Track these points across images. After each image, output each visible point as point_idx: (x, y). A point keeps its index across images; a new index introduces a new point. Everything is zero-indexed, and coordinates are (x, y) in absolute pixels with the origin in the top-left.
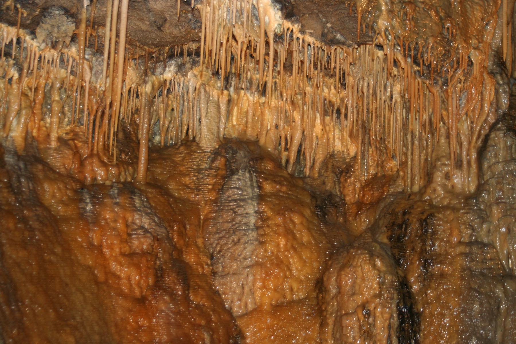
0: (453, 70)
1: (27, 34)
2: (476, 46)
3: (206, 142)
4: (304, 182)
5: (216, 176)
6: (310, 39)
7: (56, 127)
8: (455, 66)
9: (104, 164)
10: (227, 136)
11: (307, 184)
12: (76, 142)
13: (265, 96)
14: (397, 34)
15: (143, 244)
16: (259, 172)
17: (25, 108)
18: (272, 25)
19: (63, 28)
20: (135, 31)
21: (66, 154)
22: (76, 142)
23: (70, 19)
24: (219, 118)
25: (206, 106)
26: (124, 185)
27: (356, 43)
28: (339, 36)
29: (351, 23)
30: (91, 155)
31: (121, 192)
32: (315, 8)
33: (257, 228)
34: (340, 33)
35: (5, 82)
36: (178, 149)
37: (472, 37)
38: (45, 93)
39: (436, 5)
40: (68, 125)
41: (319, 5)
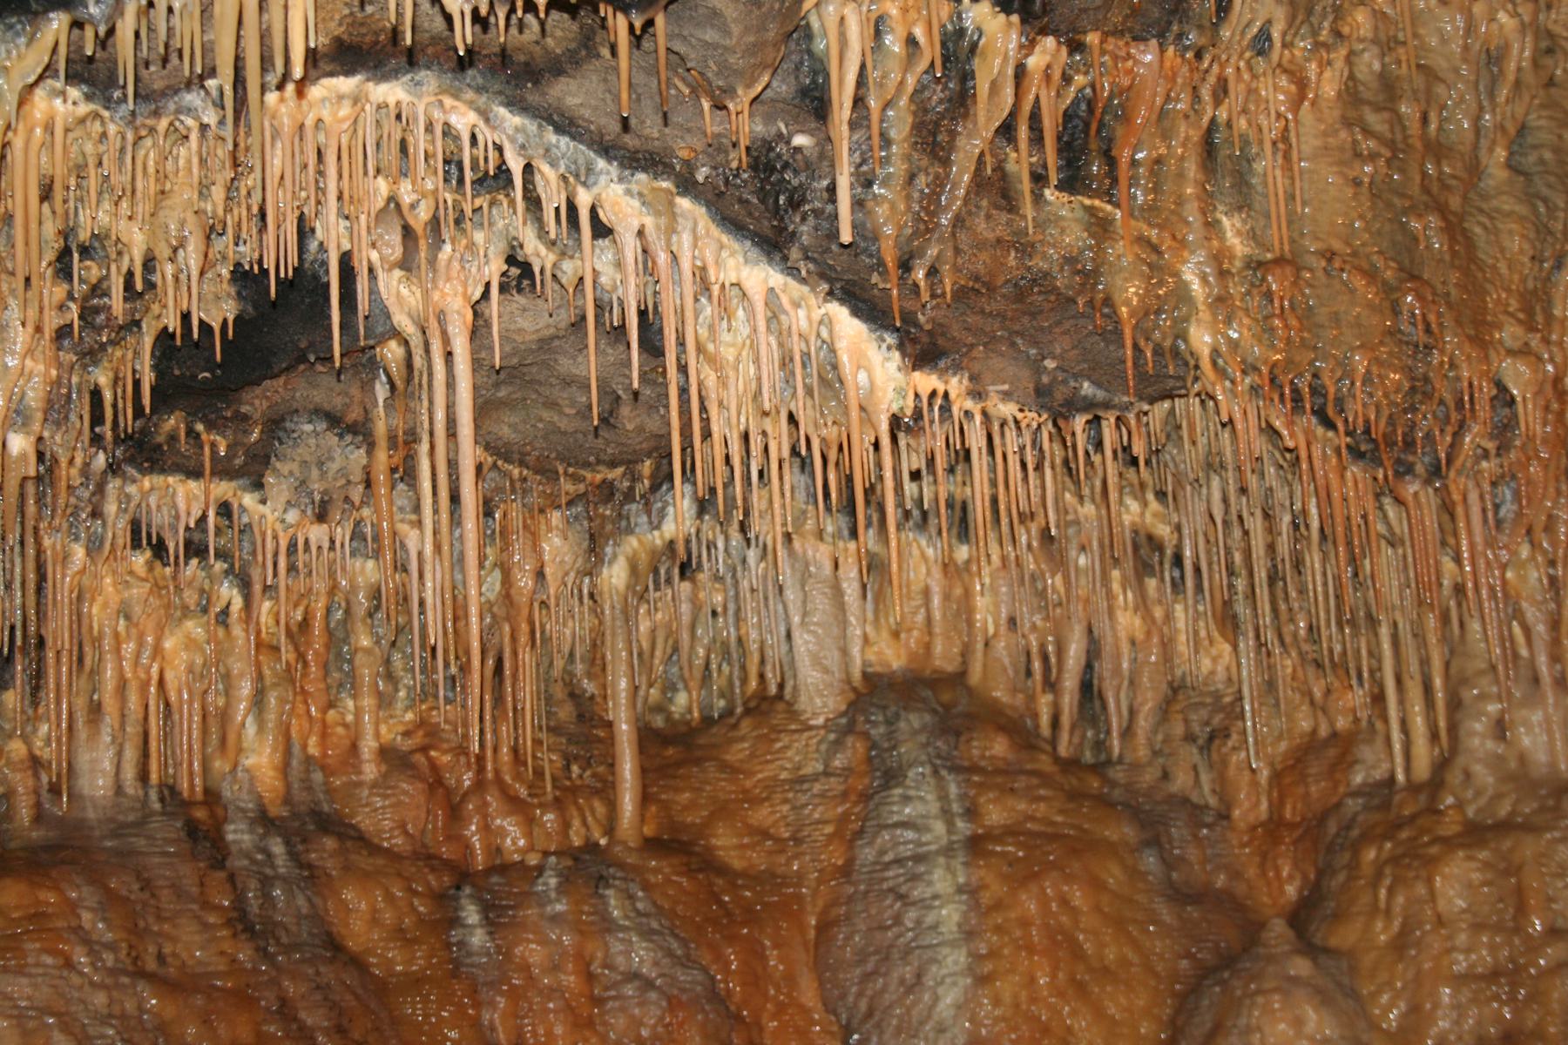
0: (1449, 429)
1: (244, 490)
2: (1516, 345)
3: (811, 699)
5: (845, 795)
7: (375, 724)
8: (1454, 416)
9: (515, 804)
10: (879, 669)
12: (433, 753)
13: (968, 542)
14: (1250, 360)
15: (640, 1024)
16: (965, 770)
17: (275, 685)
20: (545, 437)
21: (405, 793)
22: (433, 753)
23: (348, 438)
24: (844, 624)
25: (801, 595)
26: (576, 859)
27: (1141, 399)
28: (1087, 388)
29: (1112, 348)
30: (480, 785)
31: (566, 880)
32: (996, 326)
33: (969, 934)
34: (1089, 378)
35: (208, 623)
36: (735, 726)
37: (1502, 317)
38: (329, 632)
39: (1368, 249)
40: (407, 709)
41: (1004, 317)
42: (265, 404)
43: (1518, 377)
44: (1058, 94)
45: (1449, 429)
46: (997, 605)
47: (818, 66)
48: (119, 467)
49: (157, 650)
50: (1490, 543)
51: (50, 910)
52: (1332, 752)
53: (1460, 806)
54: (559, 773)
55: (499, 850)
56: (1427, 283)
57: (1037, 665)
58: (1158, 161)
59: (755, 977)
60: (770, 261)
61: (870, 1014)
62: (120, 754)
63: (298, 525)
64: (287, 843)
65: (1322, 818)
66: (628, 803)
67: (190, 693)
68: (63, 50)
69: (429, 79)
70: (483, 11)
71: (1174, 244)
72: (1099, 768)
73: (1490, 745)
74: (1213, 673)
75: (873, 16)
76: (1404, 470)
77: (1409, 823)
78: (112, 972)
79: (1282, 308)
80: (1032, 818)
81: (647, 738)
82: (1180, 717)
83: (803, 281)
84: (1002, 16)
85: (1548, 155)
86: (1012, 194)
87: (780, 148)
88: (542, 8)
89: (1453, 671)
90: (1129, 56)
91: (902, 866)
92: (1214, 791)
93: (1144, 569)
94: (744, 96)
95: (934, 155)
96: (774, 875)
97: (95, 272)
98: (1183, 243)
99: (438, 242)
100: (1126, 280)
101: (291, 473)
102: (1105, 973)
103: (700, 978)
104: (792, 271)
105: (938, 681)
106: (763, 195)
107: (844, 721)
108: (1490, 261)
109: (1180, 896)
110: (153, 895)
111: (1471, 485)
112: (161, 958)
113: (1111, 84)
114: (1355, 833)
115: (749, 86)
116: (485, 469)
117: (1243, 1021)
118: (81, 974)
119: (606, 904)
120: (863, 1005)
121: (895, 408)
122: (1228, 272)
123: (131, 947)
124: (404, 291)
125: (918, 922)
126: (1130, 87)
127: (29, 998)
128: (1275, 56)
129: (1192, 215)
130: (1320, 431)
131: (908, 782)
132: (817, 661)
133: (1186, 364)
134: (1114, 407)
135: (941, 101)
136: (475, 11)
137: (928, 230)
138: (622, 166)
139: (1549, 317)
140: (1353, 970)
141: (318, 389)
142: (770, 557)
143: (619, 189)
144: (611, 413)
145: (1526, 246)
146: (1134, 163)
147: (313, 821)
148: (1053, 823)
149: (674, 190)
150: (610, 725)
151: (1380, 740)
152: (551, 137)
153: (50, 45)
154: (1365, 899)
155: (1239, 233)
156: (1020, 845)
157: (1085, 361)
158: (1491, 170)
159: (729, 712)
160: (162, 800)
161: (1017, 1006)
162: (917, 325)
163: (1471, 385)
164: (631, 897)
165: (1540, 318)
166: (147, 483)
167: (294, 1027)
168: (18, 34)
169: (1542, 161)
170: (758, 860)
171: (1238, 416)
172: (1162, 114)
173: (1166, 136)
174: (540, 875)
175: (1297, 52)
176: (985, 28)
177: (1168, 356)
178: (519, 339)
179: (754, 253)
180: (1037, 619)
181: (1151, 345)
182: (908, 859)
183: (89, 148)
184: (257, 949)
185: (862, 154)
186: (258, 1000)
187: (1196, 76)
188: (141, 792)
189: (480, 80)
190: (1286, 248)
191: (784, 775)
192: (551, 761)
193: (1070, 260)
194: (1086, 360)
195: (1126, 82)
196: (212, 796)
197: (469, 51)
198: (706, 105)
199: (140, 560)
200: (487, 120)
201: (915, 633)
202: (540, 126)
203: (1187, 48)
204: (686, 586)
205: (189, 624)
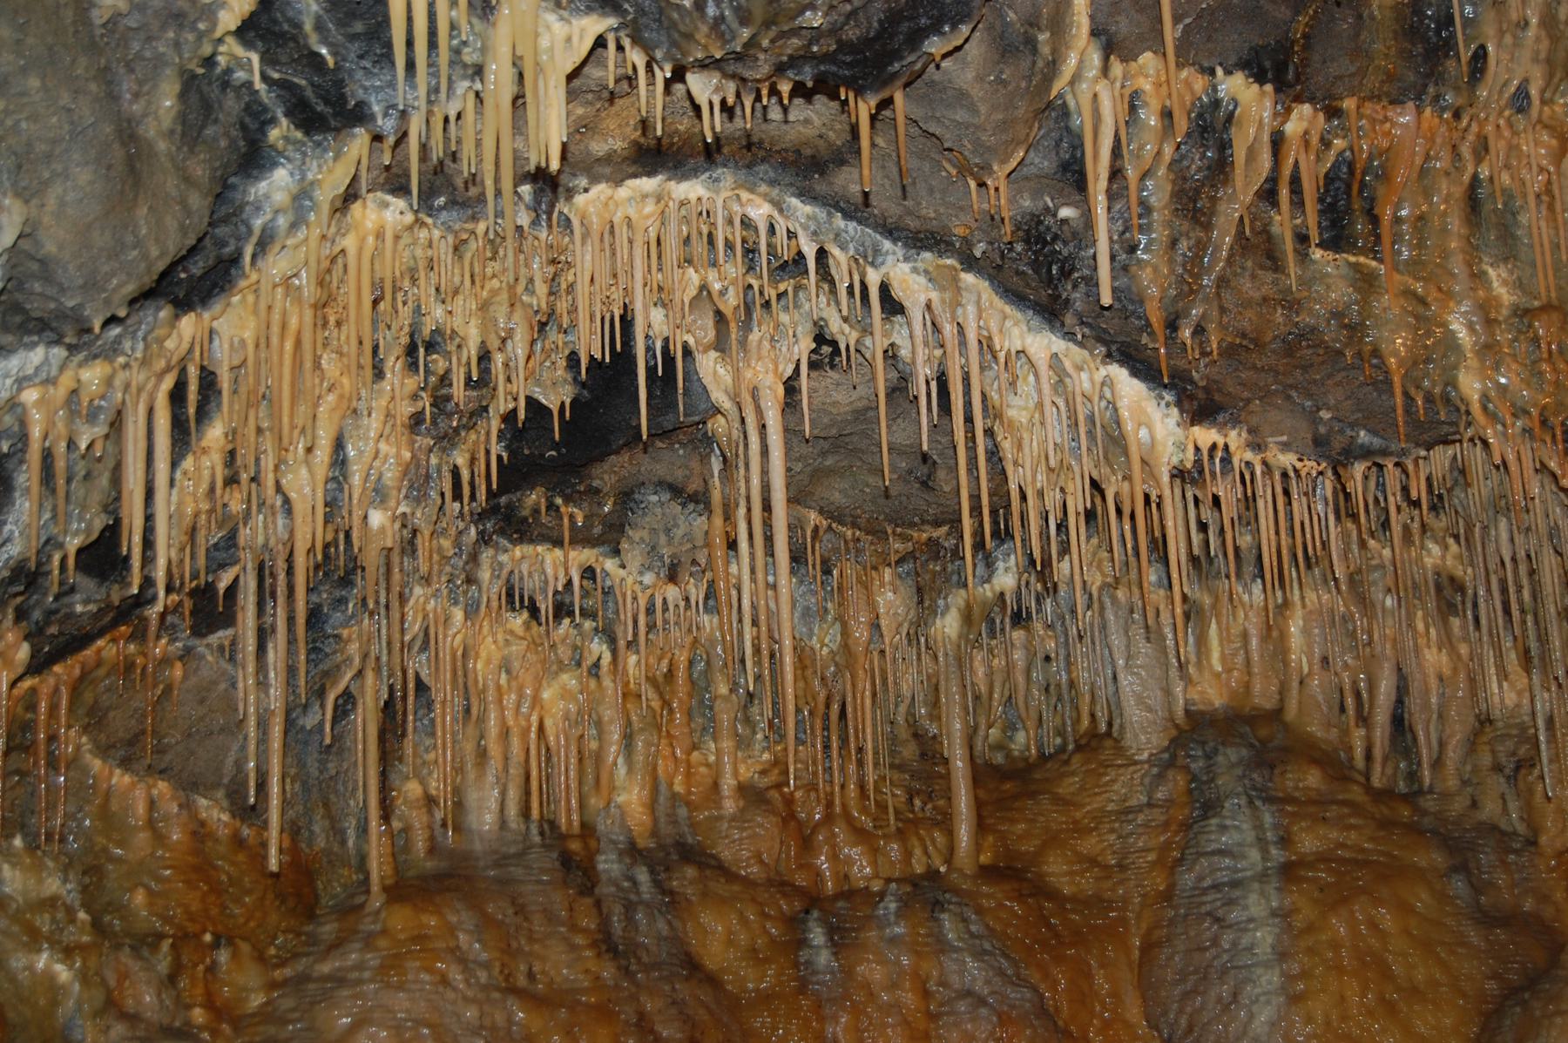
1: (605, 555)
3: (1136, 736)
4: (1417, 809)
5: (1166, 825)
6: (1287, 460)
7: (736, 766)
10: (1202, 707)
11: (1424, 813)
16: (1277, 801)
17: (642, 730)
18: (1160, 448)
19: (679, 532)
23: (691, 506)
26: (915, 885)
27: (1418, 445)
28: (1363, 436)
30: (829, 818)
32: (1270, 380)
33: (1282, 956)
34: (1365, 427)
36: (1067, 762)
40: (764, 749)
41: (1277, 373)
42: (614, 479)
44: (1318, 159)
46: (1310, 645)
47: (1076, 142)
48: (490, 538)
49: (536, 699)
51: (431, 932)
54: (902, 807)
55: (846, 876)
58: (1421, 218)
61: (1190, 1029)
62: (503, 793)
63: (655, 586)
64: (652, 872)
67: (567, 740)
68: (365, 162)
69: (727, 177)
70: (731, 101)
71: (1439, 295)
72: (1410, 798)
74: (1518, 706)
75: (1127, 92)
78: (485, 988)
79: (1550, 352)
80: (1342, 846)
81: (981, 773)
82: (1487, 748)
83: (1081, 345)
84: (1256, 87)
86: (1278, 254)
87: (1049, 221)
88: (785, 96)
90: (1386, 119)
91: (1220, 891)
92: (1521, 818)
93: (1448, 608)
94: (1001, 171)
95: (1195, 220)
97: (440, 365)
98: (1449, 295)
99: (746, 326)
100: (1393, 332)
101: (642, 539)
102: (1414, 993)
103: (1028, 995)
104: (1069, 336)
105: (1256, 718)
106: (1035, 264)
107: (1166, 756)
109: (1488, 919)
110: (526, 919)
112: (531, 976)
113: (1370, 147)
115: (1004, 162)
116: (821, 533)
118: (455, 989)
119: (941, 927)
120: (1183, 1022)
121: (1175, 460)
122: (1495, 320)
123: (503, 965)
124: (721, 371)
125: (1234, 944)
126: (1388, 150)
127: (407, 1011)
128: (1534, 112)
129: (1457, 266)
131: (1225, 812)
132: (1140, 700)
133: (1458, 410)
134: (1391, 454)
135: (1199, 169)
136: (723, 102)
137: (1192, 292)
138: (906, 245)
141: (671, 462)
142: (1096, 606)
143: (906, 267)
144: (929, 476)
146: (1398, 220)
147: (678, 853)
148: (1363, 850)
149: (959, 267)
150: (946, 761)
152: (839, 221)
153: (356, 158)
155: (1505, 283)
156: (1329, 870)
157: (1359, 411)
159: (1062, 749)
160: (542, 834)
161: (1328, 1023)
162: (1192, 382)
164: (965, 920)
166: (518, 552)
168: (325, 150)
170: (1087, 884)
171: (1511, 457)
172: (1423, 173)
173: (1427, 194)
174: (882, 900)
175: (1557, 109)
176: (1239, 97)
177: (1439, 402)
178: (835, 411)
179: (1036, 322)
181: (1421, 394)
182: (1224, 884)
183: (419, 252)
184: (619, 968)
185: (1126, 221)
186: (619, 1013)
187: (1455, 135)
188: (523, 827)
189: (772, 174)
190: (1553, 295)
192: (894, 795)
193: (1337, 315)
194: (1370, 416)
195: (1385, 144)
196: (588, 830)
197: (717, 138)
198: (973, 184)
199: (518, 621)
200: (781, 211)
201: (1235, 673)
202: (829, 214)
203: (1443, 109)
204: (1018, 635)
205: (565, 677)
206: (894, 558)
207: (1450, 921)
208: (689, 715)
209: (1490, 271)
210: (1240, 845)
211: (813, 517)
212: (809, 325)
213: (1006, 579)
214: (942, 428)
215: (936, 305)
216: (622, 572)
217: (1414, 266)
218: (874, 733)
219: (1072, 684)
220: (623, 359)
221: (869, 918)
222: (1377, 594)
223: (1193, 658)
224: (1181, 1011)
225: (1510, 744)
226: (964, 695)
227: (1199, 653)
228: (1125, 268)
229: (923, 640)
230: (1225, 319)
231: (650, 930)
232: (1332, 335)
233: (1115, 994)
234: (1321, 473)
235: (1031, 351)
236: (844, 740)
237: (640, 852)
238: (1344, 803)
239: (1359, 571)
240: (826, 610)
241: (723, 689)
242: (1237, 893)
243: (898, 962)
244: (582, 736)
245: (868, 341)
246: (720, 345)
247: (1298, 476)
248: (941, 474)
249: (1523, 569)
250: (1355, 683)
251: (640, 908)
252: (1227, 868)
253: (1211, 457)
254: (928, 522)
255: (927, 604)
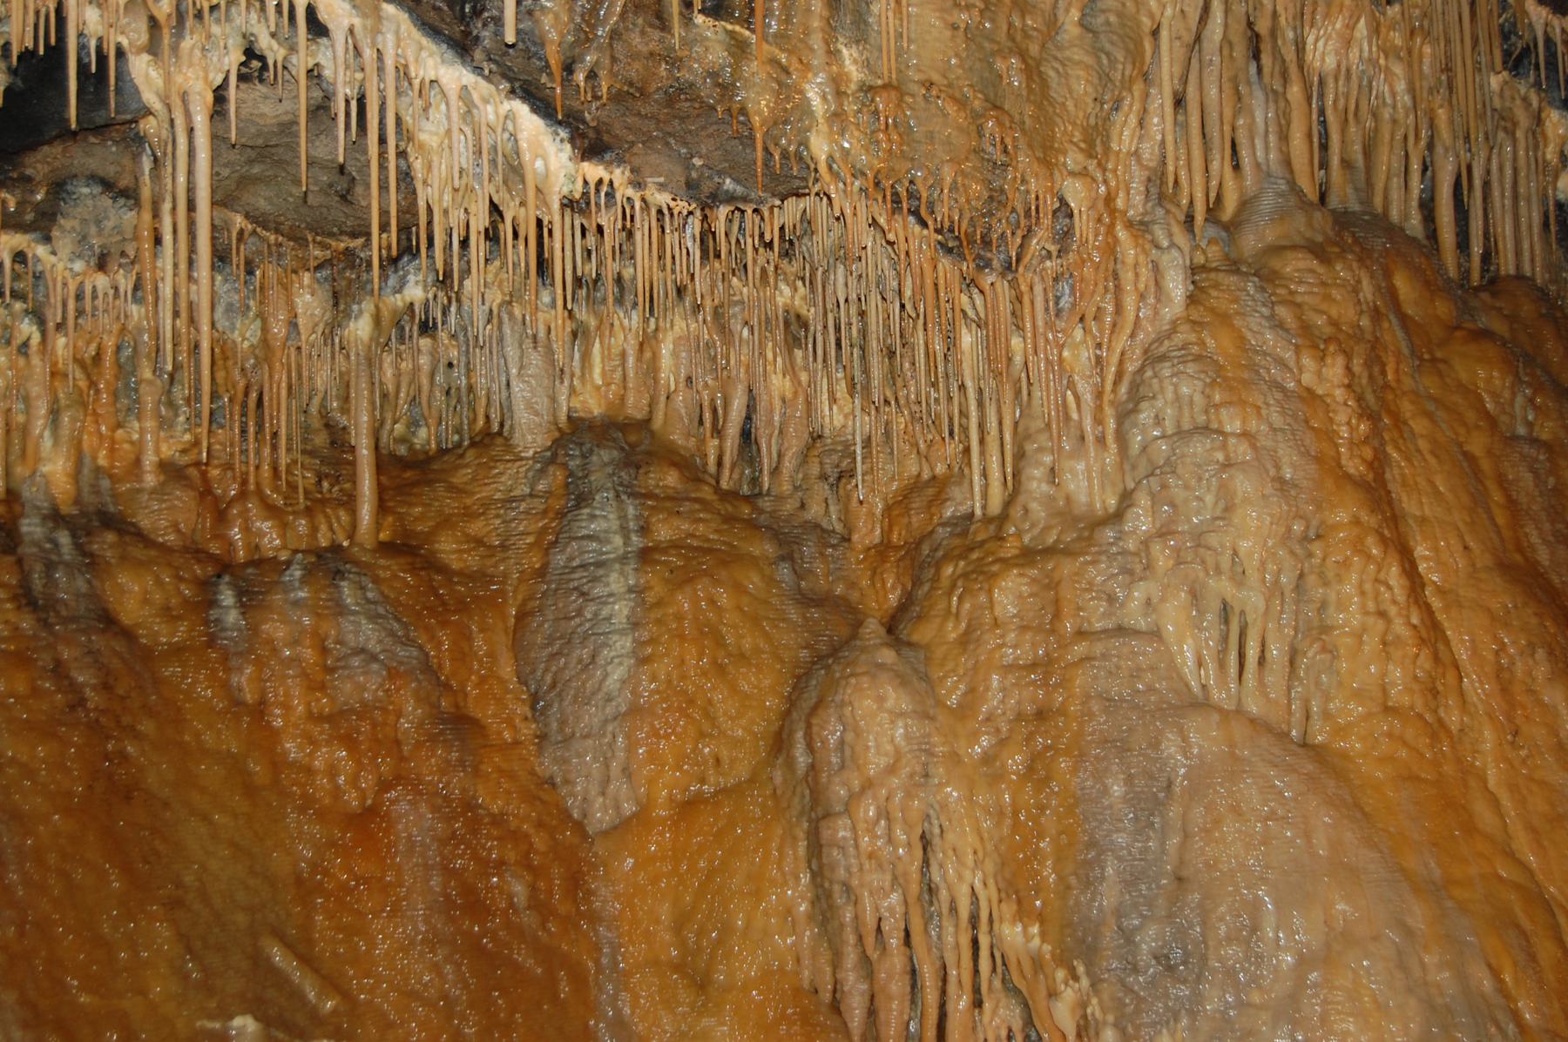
0: (1019, 233)
1: (37, 242)
2: (1078, 168)
3: (523, 436)
4: (756, 509)
5: (545, 512)
6: (663, 199)
7: (156, 442)
8: (1023, 222)
9: (271, 510)
10: (582, 414)
17: (68, 406)
18: (553, 178)
21: (178, 498)
23: (122, 201)
25: (518, 352)
26: (319, 557)
27: (774, 195)
28: (729, 184)
30: (243, 495)
31: (309, 572)
33: (635, 625)
36: (462, 456)
39: (961, 83)
40: (186, 431)
41: (658, 121)
42: (47, 169)
43: (1076, 194)
45: (1019, 233)
46: (677, 366)
50: (1050, 325)
52: (931, 491)
53: (1019, 534)
54: (312, 488)
55: (257, 547)
56: (1007, 113)
57: (707, 416)
59: (462, 655)
60: (464, 63)
61: (554, 685)
63: (85, 274)
64: (74, 536)
65: (919, 543)
66: (366, 512)
73: (1045, 487)
76: (984, 264)
77: (979, 546)
80: (692, 536)
81: (384, 462)
82: (817, 460)
83: (488, 79)
85: (1113, 19)
89: (1020, 429)
96: (485, 575)
98: (807, 67)
102: (742, 657)
104: (478, 70)
105: (627, 426)
107: (549, 454)
108: (1061, 100)
109: (807, 600)
111: (1036, 279)
114: (940, 553)
116: (246, 234)
117: (838, 698)
120: (548, 679)
121: (565, 191)
124: (153, 73)
125: (596, 614)
129: (817, 41)
130: (917, 228)
132: (530, 406)
133: (808, 167)
134: (751, 201)
137: (588, 40)
139: (1107, 149)
140: (928, 660)
141: (102, 156)
142: (495, 321)
144: (348, 191)
145: (1090, 89)
147: (99, 521)
148: (708, 540)
150: (353, 449)
151: (966, 485)
154: (942, 605)
155: (855, 62)
156: (679, 555)
158: (1067, 27)
159: (459, 445)
161: (669, 682)
162: (584, 122)
163: (1037, 198)
164: (363, 588)
165: (1099, 149)
167: (66, 683)
169: (1108, 23)
170: (472, 561)
171: (848, 211)
179: (450, 55)
180: (709, 380)
184: (39, 620)
191: (498, 496)
193: (714, 75)
204: (425, 343)
206: (313, 264)
207: (774, 600)
208: (115, 395)
209: (845, 51)
210: (606, 532)
211: (239, 221)
212: (239, 39)
213: (415, 292)
214: (357, 145)
215: (358, 30)
216: (53, 259)
217: (781, 38)
218: (289, 421)
219: (470, 388)
220: (57, 53)
221: (277, 583)
222: (736, 326)
223: (578, 372)
224: (546, 670)
225: (835, 457)
226: (372, 392)
227: (583, 368)
228: (530, 13)
229: (337, 340)
230: (616, 68)
231: (69, 587)
232: (708, 92)
233: (491, 654)
234: (690, 213)
235: (444, 81)
236: (260, 426)
237: (63, 518)
238: (696, 500)
239: (722, 305)
240: (248, 308)
241: (147, 374)
242: (601, 572)
243: (299, 622)
244: (9, 410)
245: (294, 59)
246: (153, 48)
247: (672, 215)
248: (359, 190)
249: (853, 310)
250: (713, 400)
251: (61, 567)
252: (593, 551)
253: (598, 191)
254: (346, 233)
255: (342, 307)
